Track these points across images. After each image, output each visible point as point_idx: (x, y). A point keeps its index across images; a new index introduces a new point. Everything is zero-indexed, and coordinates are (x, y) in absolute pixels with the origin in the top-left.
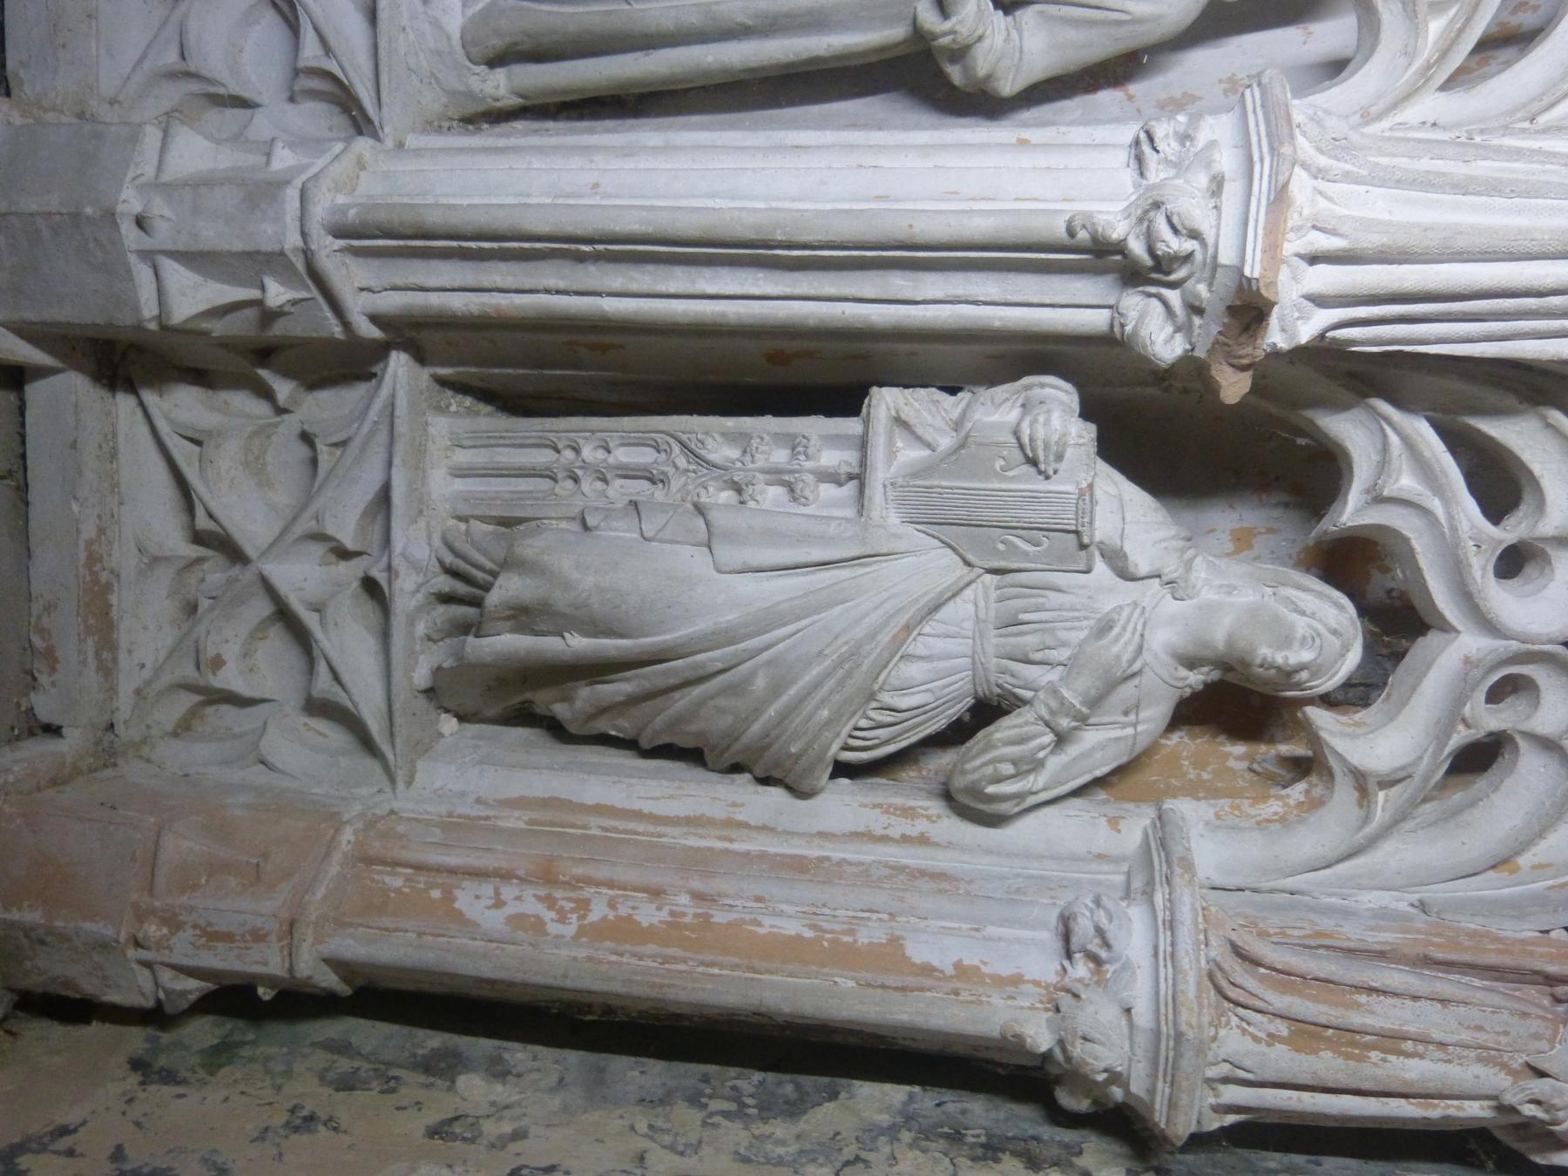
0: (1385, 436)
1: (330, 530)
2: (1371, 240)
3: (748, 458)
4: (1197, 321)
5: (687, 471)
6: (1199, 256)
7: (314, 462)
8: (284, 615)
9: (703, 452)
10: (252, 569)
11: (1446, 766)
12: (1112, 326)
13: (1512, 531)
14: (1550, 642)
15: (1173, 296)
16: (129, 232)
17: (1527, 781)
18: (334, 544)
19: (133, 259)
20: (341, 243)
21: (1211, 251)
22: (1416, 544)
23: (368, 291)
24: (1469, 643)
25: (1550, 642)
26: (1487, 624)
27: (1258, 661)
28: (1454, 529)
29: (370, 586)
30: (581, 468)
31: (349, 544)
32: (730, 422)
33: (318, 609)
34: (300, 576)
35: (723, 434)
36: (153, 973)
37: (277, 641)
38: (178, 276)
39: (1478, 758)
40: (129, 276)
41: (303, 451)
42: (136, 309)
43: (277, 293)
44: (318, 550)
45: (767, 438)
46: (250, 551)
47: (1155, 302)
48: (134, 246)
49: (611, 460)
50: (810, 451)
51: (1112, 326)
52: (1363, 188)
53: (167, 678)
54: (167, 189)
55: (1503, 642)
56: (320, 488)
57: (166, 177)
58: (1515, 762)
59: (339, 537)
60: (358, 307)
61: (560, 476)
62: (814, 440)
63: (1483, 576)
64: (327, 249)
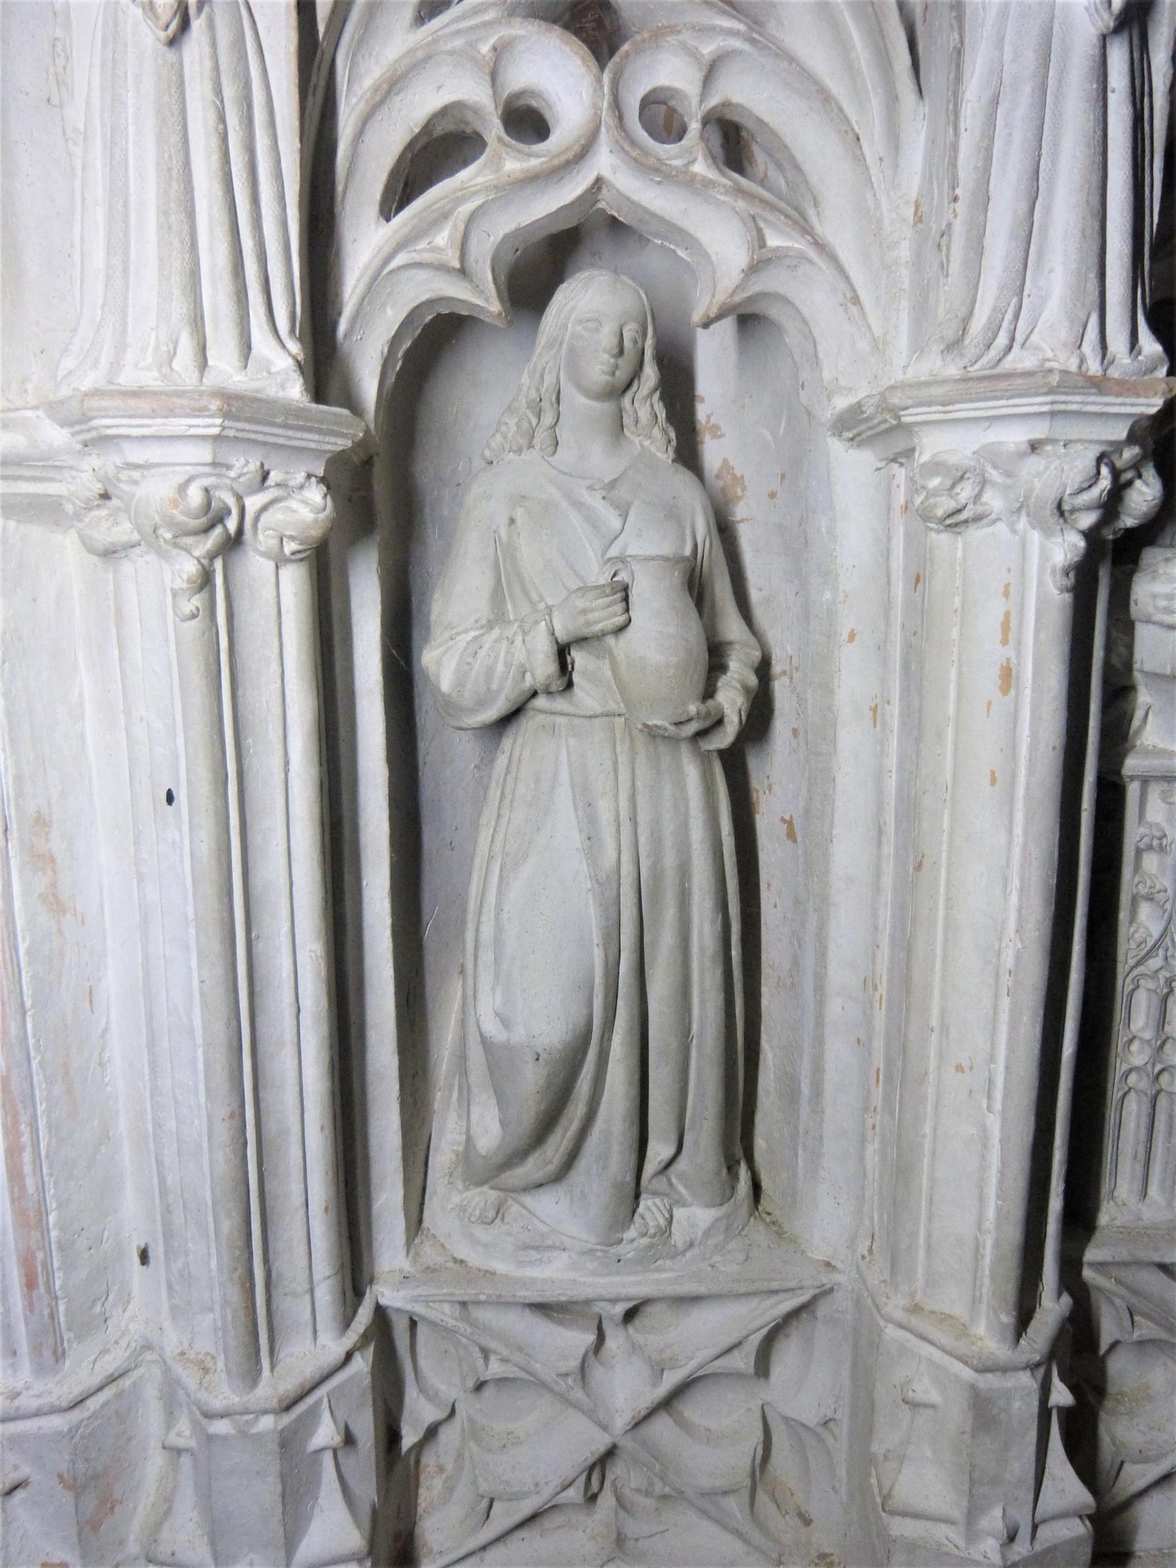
0: (400, 268)
1: (574, 1364)
2: (179, 308)
3: (1161, 897)
4: (274, 477)
5: (1166, 958)
6: (207, 482)
7: (502, 1381)
8: (667, 1403)
9: (1150, 943)
10: (622, 1442)
11: (736, 176)
12: (301, 560)
13: (493, 130)
14: (599, 80)
15: (253, 503)
16: (1021, 1549)
17: (751, 92)
18: (591, 1354)
19: (1038, 1547)
20: (266, 1372)
21: (201, 469)
22: (509, 228)
23: (316, 1341)
24: (605, 162)
25: (599, 80)
26: (583, 152)
27: (608, 378)
28: (487, 189)
29: (630, 1315)
30: (1154, 1065)
31: (591, 1338)
32: (1123, 915)
33: (658, 1370)
34: (626, 1386)
35: (1131, 922)
36: (1044, 1521)
37: (693, 1409)
38: (1050, 1500)
39: (733, 142)
40: (1051, 1550)
41: (488, 1392)
42: (1077, 1541)
43: (325, 1434)
44: (597, 1373)
45: (1137, 879)
46: (601, 1443)
47: (265, 518)
48: (1028, 1546)
49: (1148, 1035)
50: (1158, 834)
51: (301, 560)
52: (1025, 300)
53: (746, 1527)
54: (973, 1513)
55: (603, 129)
56: (535, 1376)
57: (958, 1514)
58: (738, 106)
59: (582, 1351)
60: (332, 1346)
61: (1158, 1087)
62: (1142, 830)
63: (537, 156)
64: (273, 1385)
